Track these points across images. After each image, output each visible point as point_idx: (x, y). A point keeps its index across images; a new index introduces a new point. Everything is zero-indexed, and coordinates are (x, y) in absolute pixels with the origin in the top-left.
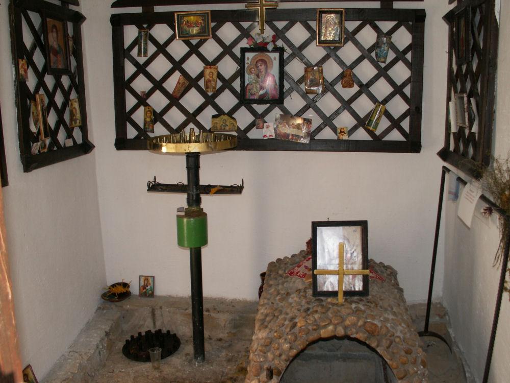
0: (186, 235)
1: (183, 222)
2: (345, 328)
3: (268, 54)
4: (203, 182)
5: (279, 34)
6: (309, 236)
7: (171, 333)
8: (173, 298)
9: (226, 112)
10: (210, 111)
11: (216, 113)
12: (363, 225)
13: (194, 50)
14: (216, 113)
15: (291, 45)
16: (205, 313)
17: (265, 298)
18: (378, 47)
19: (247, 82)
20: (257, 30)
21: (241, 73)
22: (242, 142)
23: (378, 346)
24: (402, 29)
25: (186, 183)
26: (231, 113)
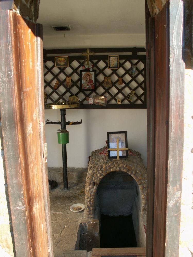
0: (61, 139)
1: (60, 134)
2: (120, 168)
3: (90, 72)
4: (67, 121)
5: (95, 65)
6: (106, 139)
7: (54, 181)
8: (54, 168)
9: (75, 94)
10: (68, 94)
11: (70, 95)
12: (125, 133)
13: (62, 70)
14: (70, 95)
15: (99, 69)
16: (68, 173)
17: (91, 162)
18: (131, 69)
19: (82, 83)
20: (86, 63)
21: (80, 80)
22: (82, 106)
23: (131, 174)
24: (141, 63)
25: (61, 121)
26: (76, 95)
